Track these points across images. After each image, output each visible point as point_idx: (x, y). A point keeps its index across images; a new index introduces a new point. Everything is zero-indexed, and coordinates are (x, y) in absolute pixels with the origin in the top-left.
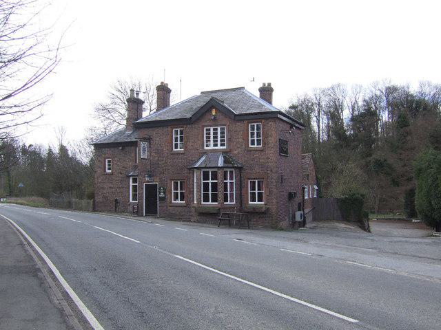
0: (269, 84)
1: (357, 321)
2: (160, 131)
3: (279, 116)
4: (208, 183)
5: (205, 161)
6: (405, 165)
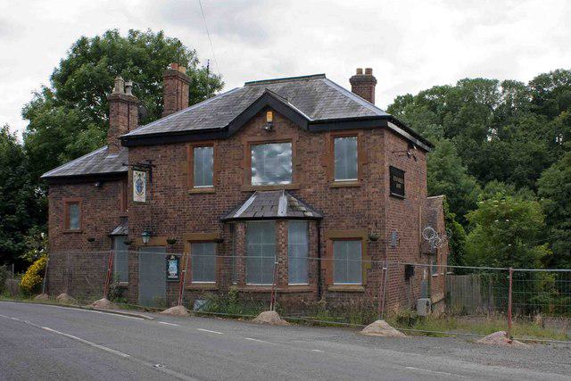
0: (369, 71)
2: (169, 151)
3: (390, 125)
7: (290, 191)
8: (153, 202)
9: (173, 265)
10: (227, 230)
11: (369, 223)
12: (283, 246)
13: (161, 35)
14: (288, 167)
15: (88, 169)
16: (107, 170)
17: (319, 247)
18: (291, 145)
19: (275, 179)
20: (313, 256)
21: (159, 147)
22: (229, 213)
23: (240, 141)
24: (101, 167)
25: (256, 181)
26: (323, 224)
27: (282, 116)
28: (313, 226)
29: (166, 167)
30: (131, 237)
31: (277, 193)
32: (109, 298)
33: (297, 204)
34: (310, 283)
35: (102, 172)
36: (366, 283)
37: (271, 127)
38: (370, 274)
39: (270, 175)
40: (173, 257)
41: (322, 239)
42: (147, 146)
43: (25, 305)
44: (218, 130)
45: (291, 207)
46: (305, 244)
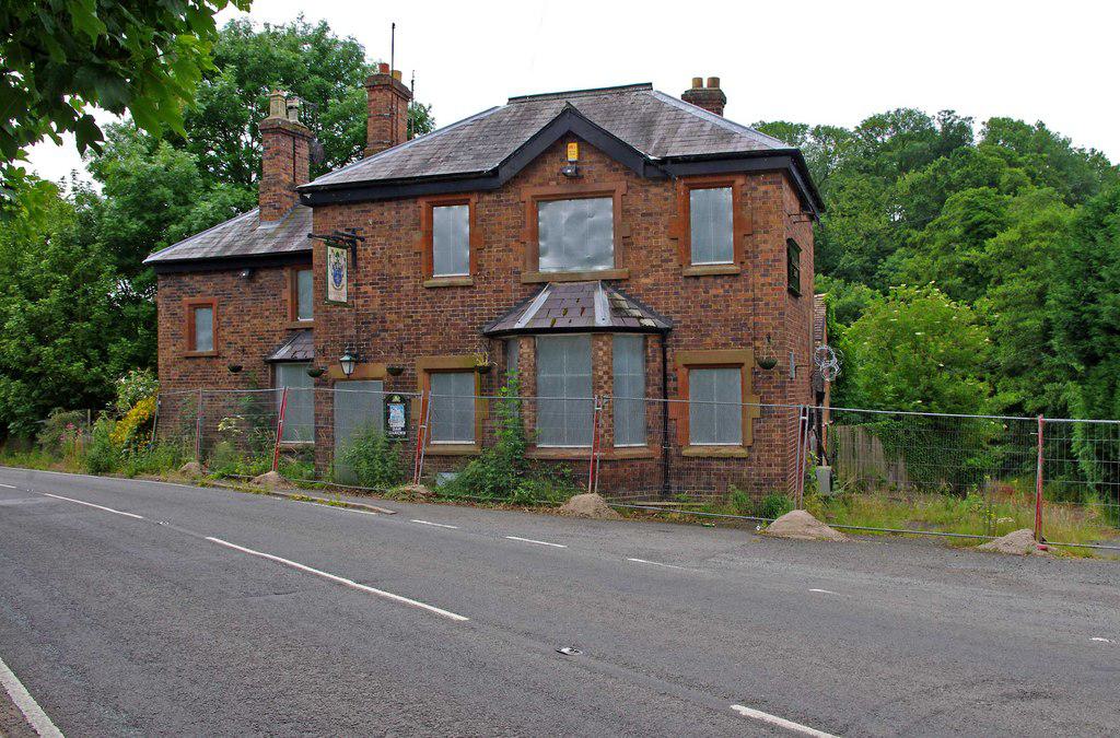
0: (715, 81)
1: (735, 707)
2: (388, 213)
4: (1069, 429)
5: (546, 309)
6: (583, 309)
7: (609, 283)
8: (361, 301)
9: (397, 412)
10: (498, 349)
11: (755, 339)
12: (606, 378)
13: (325, 28)
14: (606, 241)
15: (228, 247)
16: (262, 248)
17: (665, 380)
18: (610, 202)
19: (582, 263)
20: (654, 396)
21: (369, 206)
22: (498, 321)
23: (519, 194)
24: (252, 243)
25: (548, 264)
26: (670, 341)
27: (597, 151)
28: (653, 341)
29: (381, 240)
30: (320, 363)
31: (588, 286)
32: (604, 491)
33: (625, 304)
34: (649, 442)
35: (253, 252)
36: (749, 444)
37: (577, 170)
38: (757, 426)
39: (567, 252)
40: (396, 399)
41: (670, 366)
42: (349, 203)
43: (370, 510)
44: (479, 175)
45: (616, 310)
46: (640, 375)
